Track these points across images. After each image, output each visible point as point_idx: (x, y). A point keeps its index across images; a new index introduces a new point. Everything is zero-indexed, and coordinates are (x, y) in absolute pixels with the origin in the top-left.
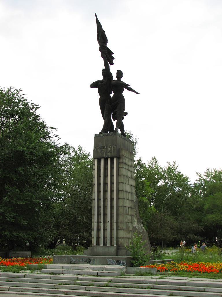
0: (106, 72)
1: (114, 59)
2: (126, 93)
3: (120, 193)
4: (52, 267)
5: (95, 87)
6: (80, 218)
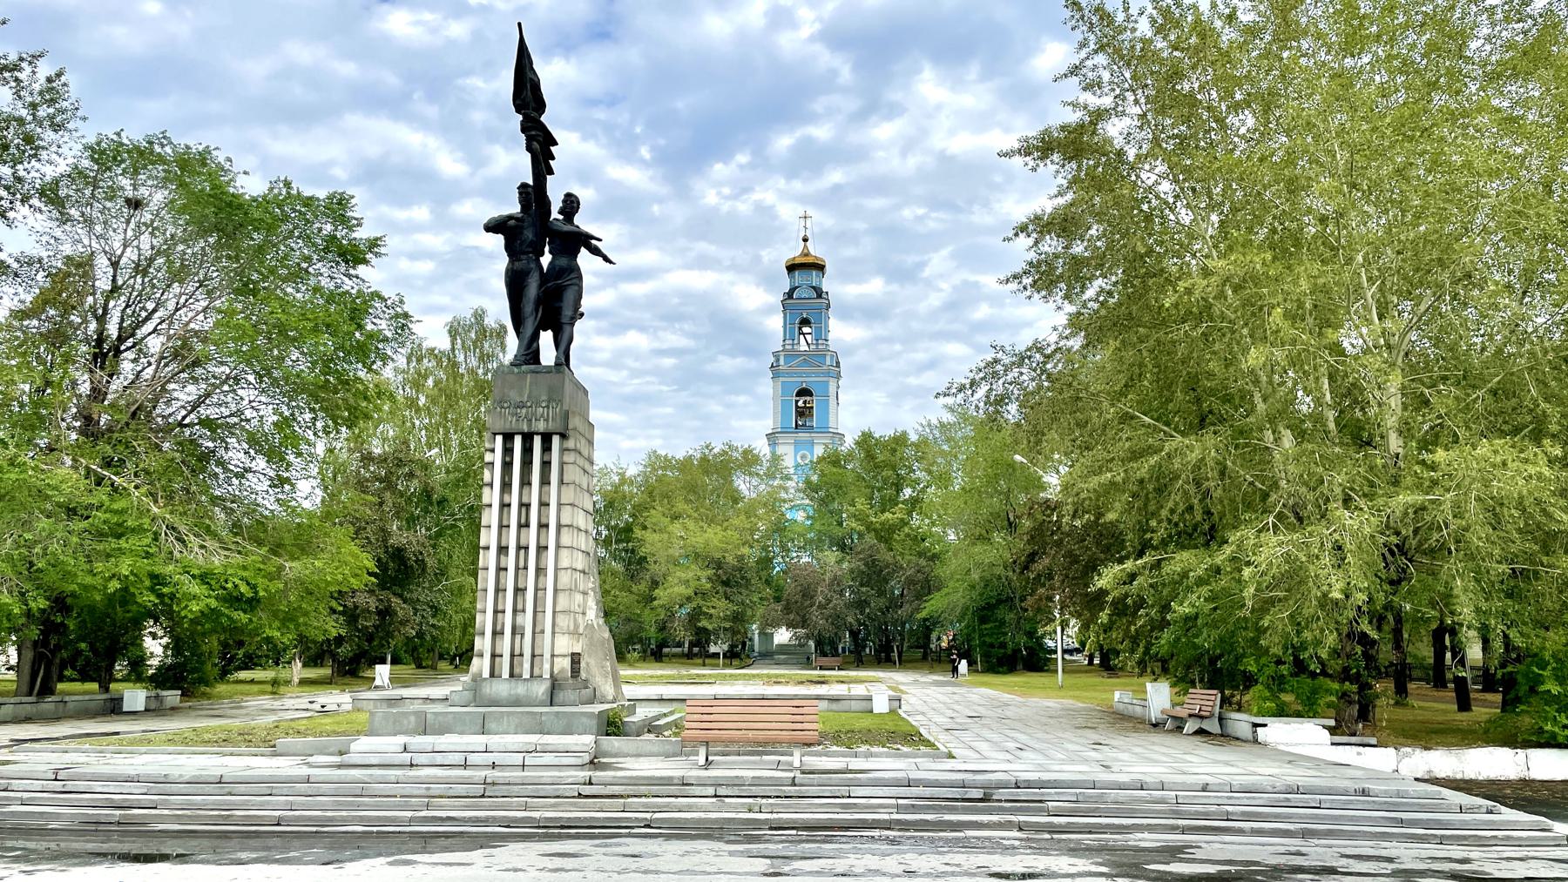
0: (533, 196)
1: (553, 158)
2: (584, 259)
3: (564, 531)
4: (1278, 732)
5: (496, 232)
6: (292, 598)
